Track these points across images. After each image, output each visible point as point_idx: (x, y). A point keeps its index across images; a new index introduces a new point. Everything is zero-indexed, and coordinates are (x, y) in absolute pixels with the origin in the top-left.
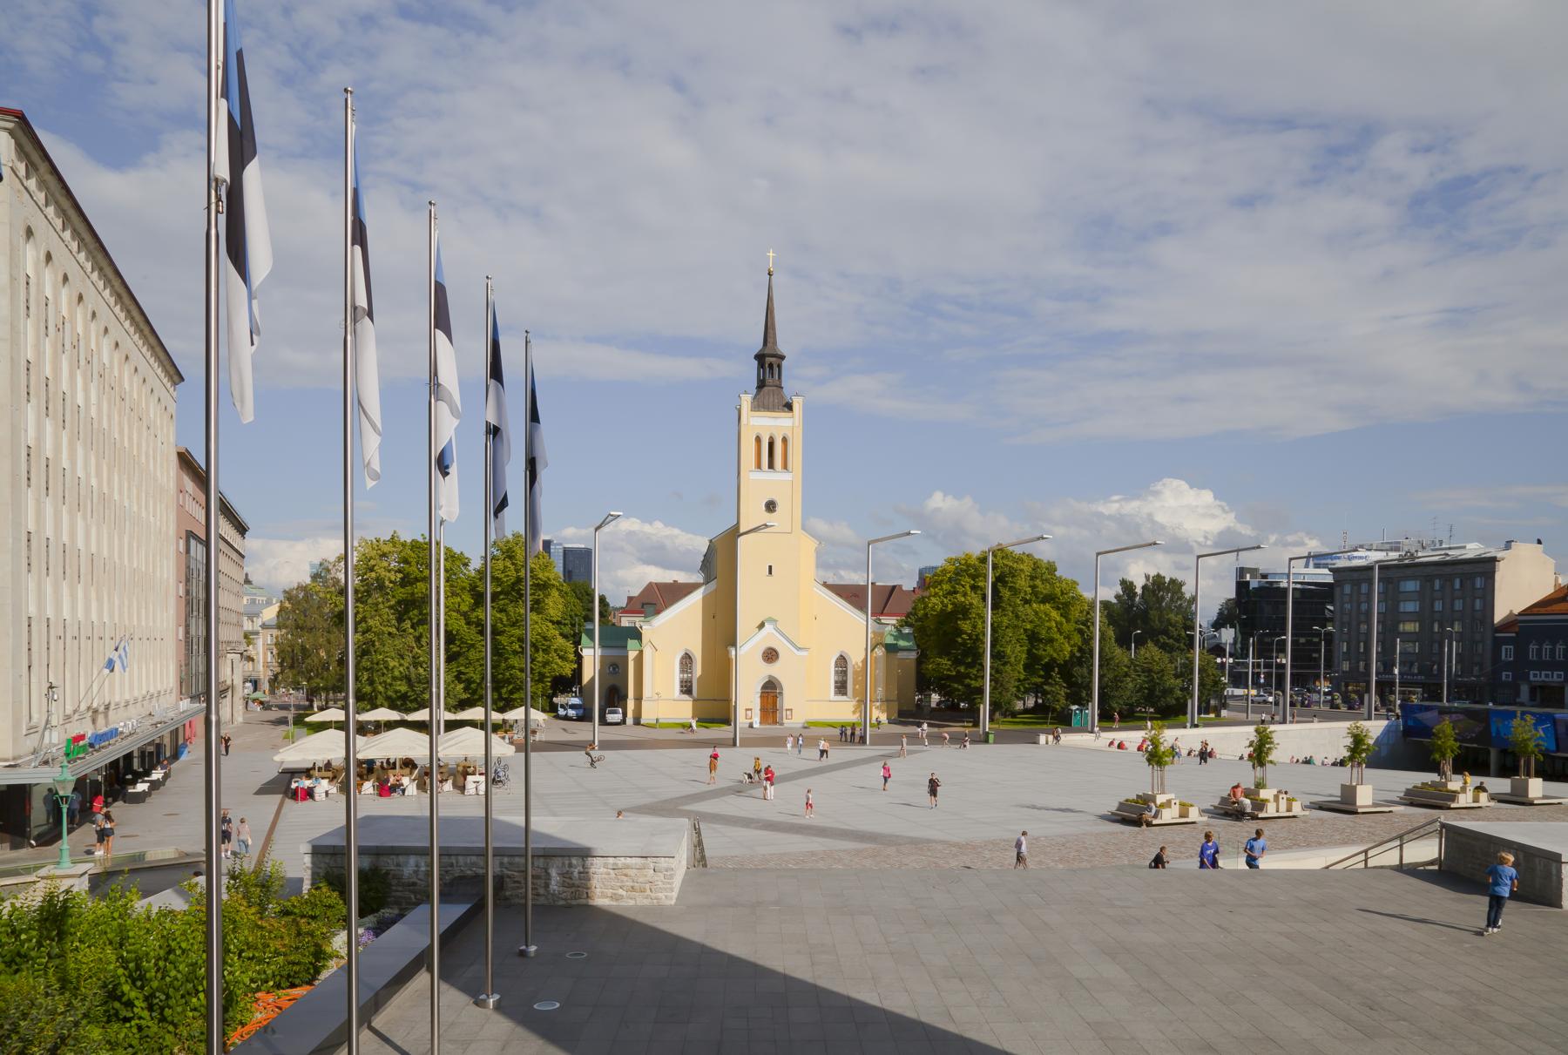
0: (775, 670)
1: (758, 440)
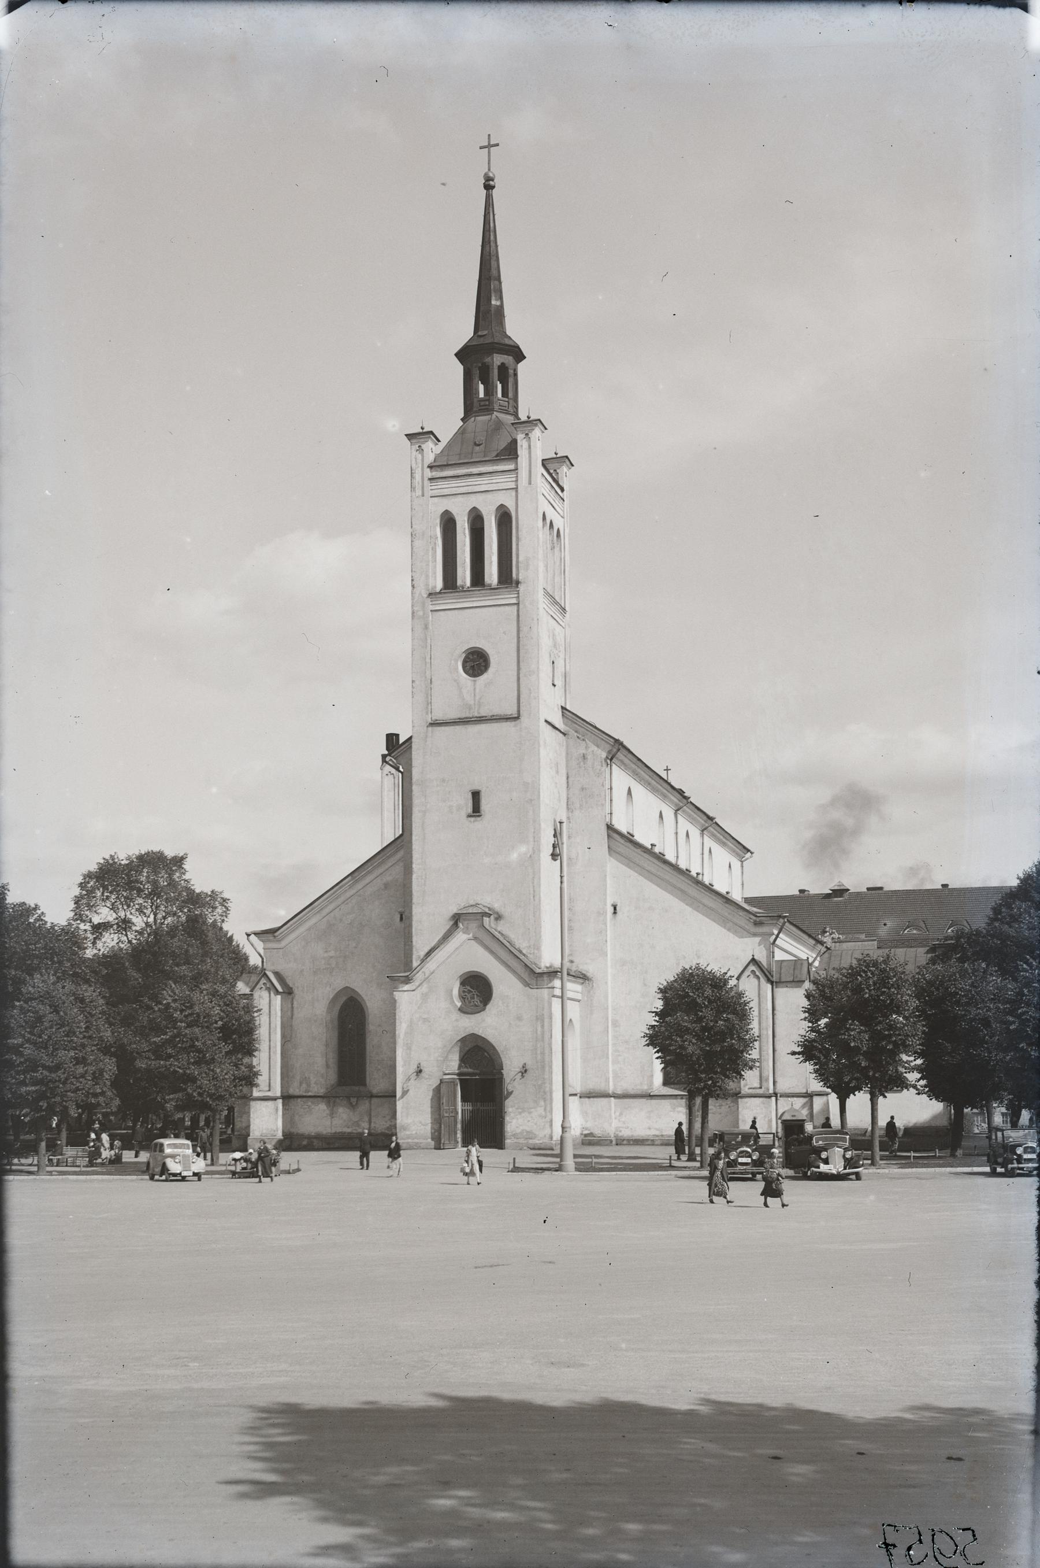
0: (489, 1025)
1: (448, 523)
